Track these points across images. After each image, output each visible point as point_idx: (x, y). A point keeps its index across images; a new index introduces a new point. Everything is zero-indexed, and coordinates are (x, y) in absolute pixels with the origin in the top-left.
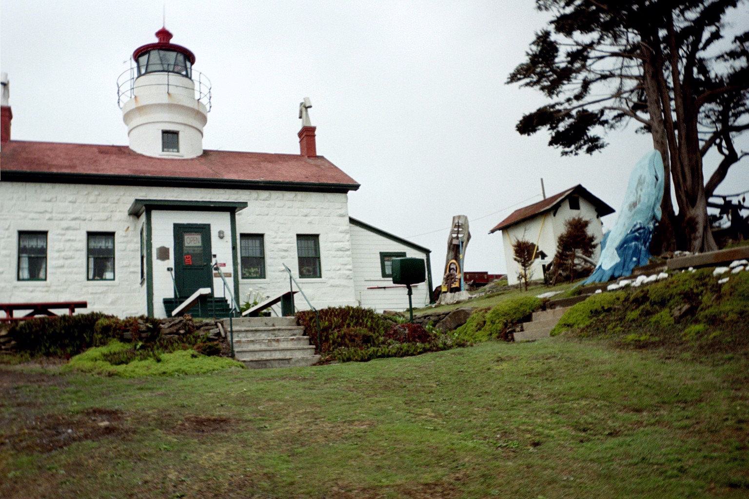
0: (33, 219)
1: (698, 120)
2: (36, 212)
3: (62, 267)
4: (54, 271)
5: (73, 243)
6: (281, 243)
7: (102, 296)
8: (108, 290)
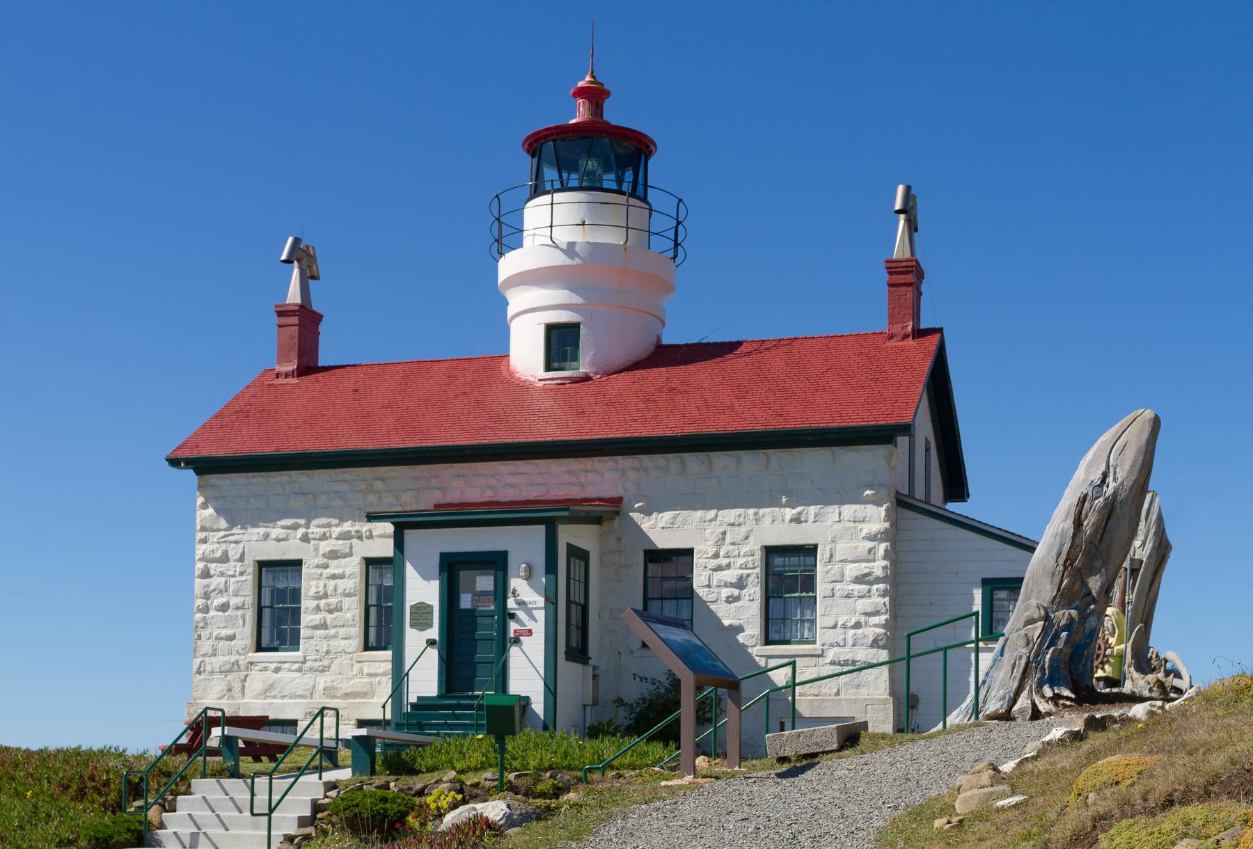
0: (278, 540)
1: (721, 512)
3: (324, 626)
6: (728, 566)
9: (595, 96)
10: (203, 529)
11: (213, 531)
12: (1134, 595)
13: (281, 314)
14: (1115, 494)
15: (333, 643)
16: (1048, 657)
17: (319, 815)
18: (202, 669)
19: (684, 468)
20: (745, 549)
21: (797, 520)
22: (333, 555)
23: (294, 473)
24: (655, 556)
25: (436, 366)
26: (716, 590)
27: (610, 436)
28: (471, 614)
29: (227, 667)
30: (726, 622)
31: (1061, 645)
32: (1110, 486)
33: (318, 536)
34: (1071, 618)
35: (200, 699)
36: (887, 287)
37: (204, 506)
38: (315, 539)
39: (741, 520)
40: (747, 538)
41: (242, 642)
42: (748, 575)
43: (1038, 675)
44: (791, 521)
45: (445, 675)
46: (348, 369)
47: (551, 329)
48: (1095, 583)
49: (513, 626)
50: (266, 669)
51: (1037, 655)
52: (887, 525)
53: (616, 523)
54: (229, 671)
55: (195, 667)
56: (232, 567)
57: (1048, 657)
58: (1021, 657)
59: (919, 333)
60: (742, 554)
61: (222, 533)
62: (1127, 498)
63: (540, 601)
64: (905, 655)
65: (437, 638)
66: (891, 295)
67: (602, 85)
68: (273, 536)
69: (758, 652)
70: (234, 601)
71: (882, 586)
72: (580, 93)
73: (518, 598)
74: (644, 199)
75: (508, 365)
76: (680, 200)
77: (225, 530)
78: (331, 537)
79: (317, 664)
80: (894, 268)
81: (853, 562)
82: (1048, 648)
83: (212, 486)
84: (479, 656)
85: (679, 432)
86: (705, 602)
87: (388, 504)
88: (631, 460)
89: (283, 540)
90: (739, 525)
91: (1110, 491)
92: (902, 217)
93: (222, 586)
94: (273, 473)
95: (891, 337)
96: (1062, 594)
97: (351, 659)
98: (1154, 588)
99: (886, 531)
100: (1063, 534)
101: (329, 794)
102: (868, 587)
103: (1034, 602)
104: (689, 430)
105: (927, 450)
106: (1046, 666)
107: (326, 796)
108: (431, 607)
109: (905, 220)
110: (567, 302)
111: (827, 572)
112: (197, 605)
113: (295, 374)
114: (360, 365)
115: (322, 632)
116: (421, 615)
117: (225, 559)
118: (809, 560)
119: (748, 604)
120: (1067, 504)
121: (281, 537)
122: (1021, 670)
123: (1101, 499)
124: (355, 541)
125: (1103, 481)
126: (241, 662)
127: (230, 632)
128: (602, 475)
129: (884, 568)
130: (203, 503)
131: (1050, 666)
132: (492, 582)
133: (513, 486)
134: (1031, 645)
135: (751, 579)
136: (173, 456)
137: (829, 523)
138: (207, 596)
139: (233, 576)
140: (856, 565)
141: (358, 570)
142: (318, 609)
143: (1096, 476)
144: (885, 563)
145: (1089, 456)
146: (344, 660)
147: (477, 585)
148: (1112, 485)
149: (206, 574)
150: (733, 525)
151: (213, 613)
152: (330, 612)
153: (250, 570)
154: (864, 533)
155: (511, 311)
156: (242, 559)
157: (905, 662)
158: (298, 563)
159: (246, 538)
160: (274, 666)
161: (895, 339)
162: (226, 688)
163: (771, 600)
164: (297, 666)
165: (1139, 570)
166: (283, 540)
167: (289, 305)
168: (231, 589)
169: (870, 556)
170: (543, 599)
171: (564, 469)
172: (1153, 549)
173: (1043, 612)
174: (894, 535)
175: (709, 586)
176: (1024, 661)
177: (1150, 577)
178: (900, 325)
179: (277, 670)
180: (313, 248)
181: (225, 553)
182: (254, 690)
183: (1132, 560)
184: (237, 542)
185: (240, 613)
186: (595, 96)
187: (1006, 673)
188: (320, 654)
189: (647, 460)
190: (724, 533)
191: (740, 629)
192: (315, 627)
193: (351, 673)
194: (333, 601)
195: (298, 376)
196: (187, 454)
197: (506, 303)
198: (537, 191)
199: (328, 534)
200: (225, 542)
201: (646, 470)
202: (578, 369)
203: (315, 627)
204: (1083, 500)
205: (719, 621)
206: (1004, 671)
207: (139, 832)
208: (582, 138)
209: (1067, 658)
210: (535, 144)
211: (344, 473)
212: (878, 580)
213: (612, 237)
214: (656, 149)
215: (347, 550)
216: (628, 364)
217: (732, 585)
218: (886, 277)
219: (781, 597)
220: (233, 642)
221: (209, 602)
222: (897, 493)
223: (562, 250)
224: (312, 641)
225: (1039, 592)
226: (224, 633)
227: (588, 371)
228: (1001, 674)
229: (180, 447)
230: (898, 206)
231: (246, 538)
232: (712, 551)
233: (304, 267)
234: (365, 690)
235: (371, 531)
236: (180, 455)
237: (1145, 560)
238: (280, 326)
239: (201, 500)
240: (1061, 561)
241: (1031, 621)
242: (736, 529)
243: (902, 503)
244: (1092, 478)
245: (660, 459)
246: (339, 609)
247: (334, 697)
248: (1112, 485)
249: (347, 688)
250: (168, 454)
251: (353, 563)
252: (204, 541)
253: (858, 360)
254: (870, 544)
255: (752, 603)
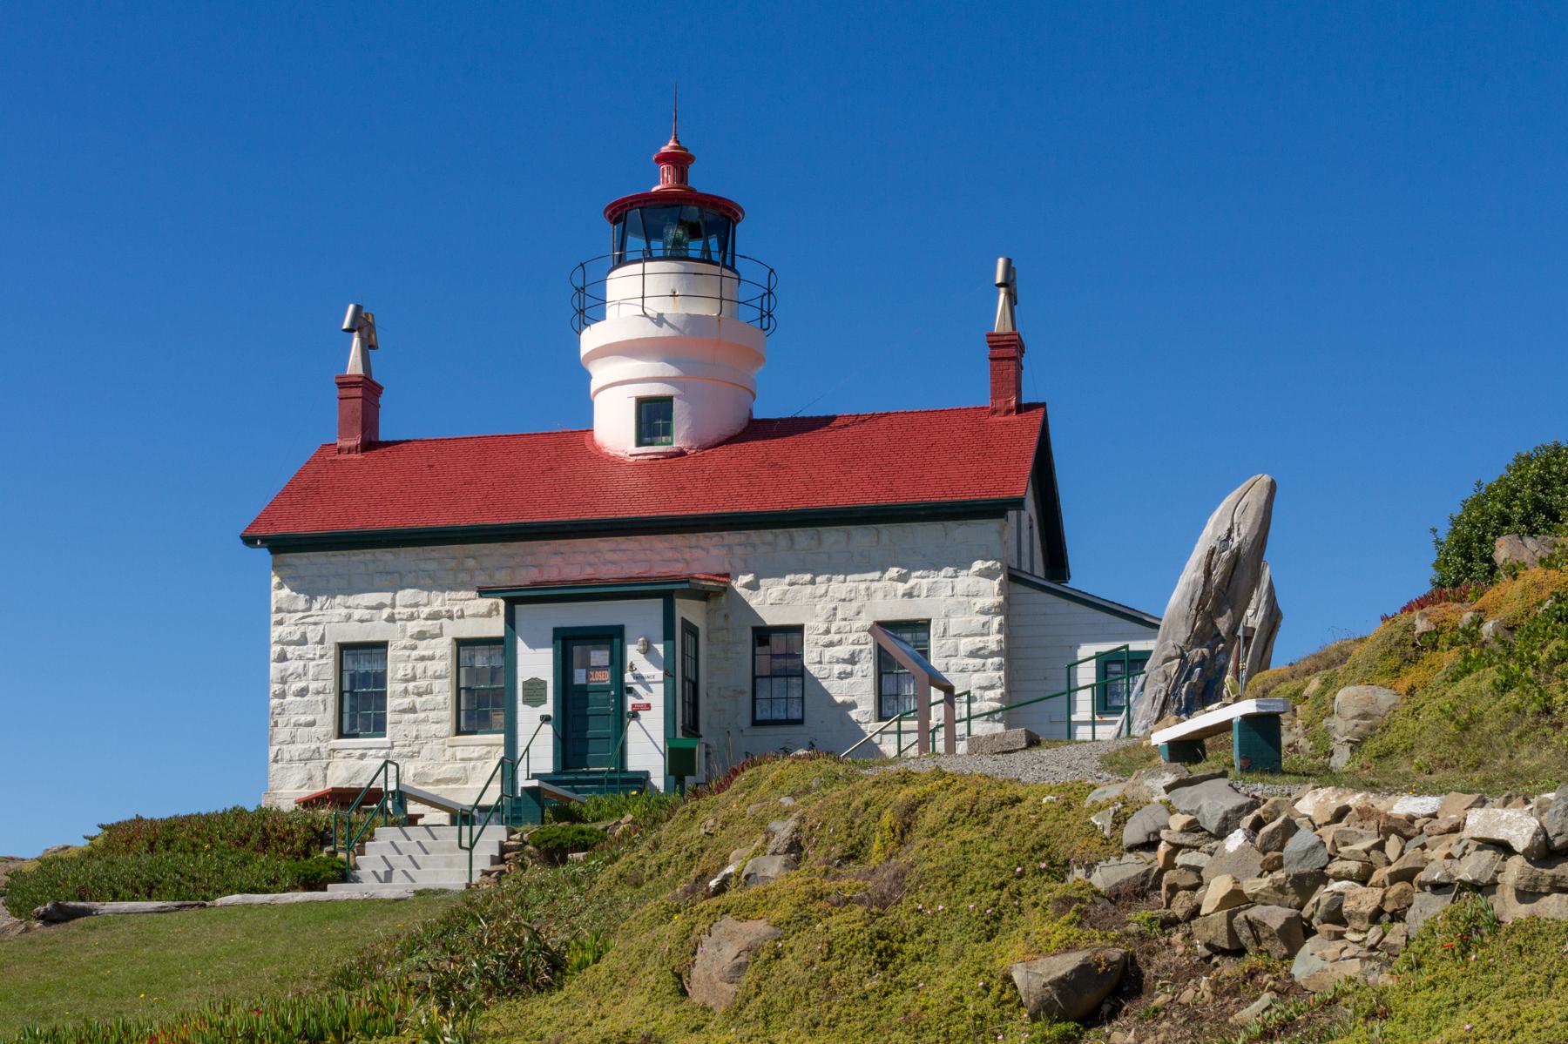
0: (361, 621)
2: (367, 608)
3: (413, 710)
4: (397, 717)
5: (429, 663)
6: (840, 642)
7: (479, 764)
8: (489, 752)
9: (680, 161)
10: (279, 610)
11: (289, 612)
12: (1248, 661)
13: (342, 385)
14: (1239, 548)
15: (423, 727)
16: (1184, 690)
17: (507, 856)
18: (279, 757)
19: (792, 544)
20: (857, 624)
21: (909, 595)
22: (422, 636)
23: (378, 551)
24: (763, 634)
25: (513, 441)
26: (828, 666)
27: (717, 511)
28: (583, 690)
29: (307, 755)
30: (839, 699)
31: (1194, 678)
32: (1235, 541)
33: (405, 617)
34: (1203, 655)
35: (277, 788)
36: (989, 362)
37: (280, 586)
38: (401, 620)
39: (853, 595)
40: (858, 613)
41: (323, 729)
42: (861, 651)
43: (1176, 706)
44: (904, 595)
45: (560, 751)
46: (416, 444)
47: (642, 403)
48: (1223, 624)
49: (631, 701)
50: (350, 756)
51: (1174, 689)
52: (1001, 599)
53: (723, 599)
54: (309, 759)
55: (272, 756)
56: (311, 650)
57: (1184, 690)
58: (1160, 691)
59: (1021, 408)
60: (854, 630)
61: (301, 615)
62: (1250, 550)
63: (659, 674)
64: (1065, 688)
65: (551, 714)
66: (993, 369)
67: (686, 150)
68: (356, 617)
69: (870, 727)
70: (313, 686)
71: (997, 660)
72: (664, 158)
73: (636, 672)
74: (732, 268)
75: (593, 440)
76: (772, 270)
77: (303, 611)
78: (419, 617)
79: (407, 749)
80: (995, 342)
81: (967, 636)
82: (1184, 682)
83: (289, 565)
84: (591, 732)
85: (789, 507)
86: (816, 678)
87: (502, 578)
88: (738, 536)
89: (367, 621)
90: (851, 600)
91: (1235, 545)
92: (1002, 290)
93: (300, 670)
94: (356, 551)
95: (994, 412)
96: (1196, 634)
97: (443, 744)
98: (1266, 656)
99: (1000, 606)
100: (1195, 582)
101: (512, 837)
102: (982, 661)
103: (1170, 642)
104: (799, 505)
105: (1031, 527)
106: (1183, 698)
107: (509, 840)
108: (545, 682)
109: (1006, 294)
110: (659, 375)
111: (941, 647)
112: (272, 691)
113: (359, 449)
114: (415, 440)
115: (411, 716)
116: (534, 692)
117: (303, 641)
118: (922, 635)
119: (861, 680)
120: (1198, 557)
121: (365, 617)
122: (1161, 702)
123: (1228, 552)
124: (445, 621)
125: (1229, 536)
126: (322, 750)
127: (310, 718)
128: (708, 552)
129: (999, 642)
130: (279, 583)
131: (1186, 699)
132: (607, 657)
133: (613, 563)
134: (1169, 680)
135: (863, 655)
136: (248, 534)
137: (942, 598)
138: (283, 681)
139: (314, 659)
140: (970, 639)
141: (449, 651)
142: (406, 691)
143: (1223, 533)
144: (1001, 637)
145: (1217, 514)
146: (435, 745)
147: (592, 660)
148: (1237, 540)
149: (282, 658)
150: (844, 600)
151: (290, 698)
152: (420, 695)
153: (332, 652)
154: (977, 608)
155: (594, 386)
156: (322, 641)
157: (1066, 696)
158: (383, 645)
159: (326, 619)
160: (359, 752)
161: (998, 414)
162: (306, 777)
163: (884, 676)
164: (384, 752)
165: (1251, 638)
166: (367, 621)
167: (350, 376)
168: (311, 673)
169: (984, 631)
170: (662, 672)
171: (667, 545)
172: (1265, 616)
173: (1179, 651)
174: (1006, 608)
175: (820, 662)
176: (1163, 694)
177: (1262, 645)
178: (1002, 400)
179: (362, 757)
180: (372, 315)
181: (304, 636)
182: (338, 778)
183: (1246, 628)
184: (315, 624)
185: (320, 697)
186: (680, 161)
187: (1148, 705)
188: (409, 739)
189: (754, 535)
190: (835, 609)
191: (853, 705)
192: (404, 711)
193: (443, 759)
194: (422, 684)
195: (362, 452)
196: (263, 532)
197: (588, 377)
198: (621, 262)
199: (416, 615)
200: (303, 623)
201: (754, 546)
202: (671, 443)
203: (404, 711)
204: (1212, 552)
205: (831, 698)
206: (1146, 703)
207: (342, 870)
208: (667, 206)
209: (1200, 691)
210: (618, 213)
211: (433, 551)
212: (993, 654)
213: (707, 309)
214: (743, 214)
215: (438, 631)
216: (722, 439)
217: (844, 661)
218: (988, 350)
219: (892, 673)
220: (313, 729)
221: (286, 687)
222: (1009, 567)
223: (652, 319)
224: (400, 726)
225: (1175, 634)
226: (303, 719)
227: (682, 446)
228: (1143, 707)
229: (252, 526)
230: (999, 279)
231: (326, 619)
232: (822, 628)
233: (365, 336)
234: (458, 776)
235: (462, 611)
236: (254, 532)
237: (1257, 627)
238: (341, 399)
239: (275, 580)
240: (1194, 606)
241: (1169, 659)
242: (847, 604)
243: (1014, 578)
244: (1219, 534)
245: (767, 535)
246: (429, 692)
247: (426, 783)
248: (1237, 540)
249: (439, 774)
250: (242, 531)
251: (444, 644)
252: (280, 623)
253: (963, 435)
254: (984, 618)
255: (864, 679)
